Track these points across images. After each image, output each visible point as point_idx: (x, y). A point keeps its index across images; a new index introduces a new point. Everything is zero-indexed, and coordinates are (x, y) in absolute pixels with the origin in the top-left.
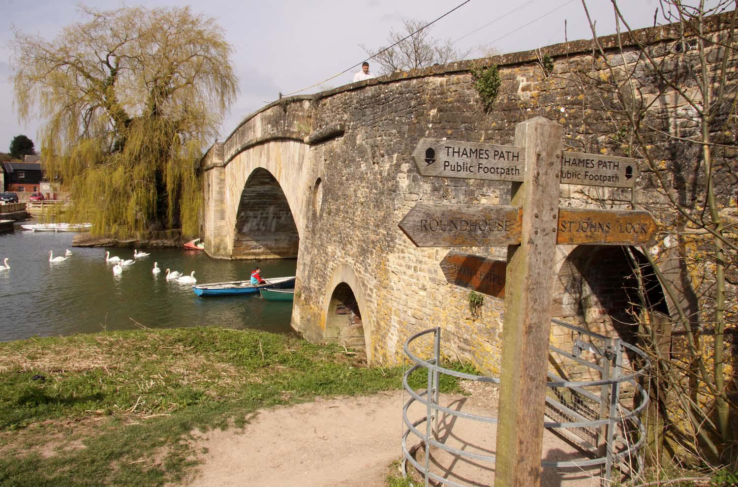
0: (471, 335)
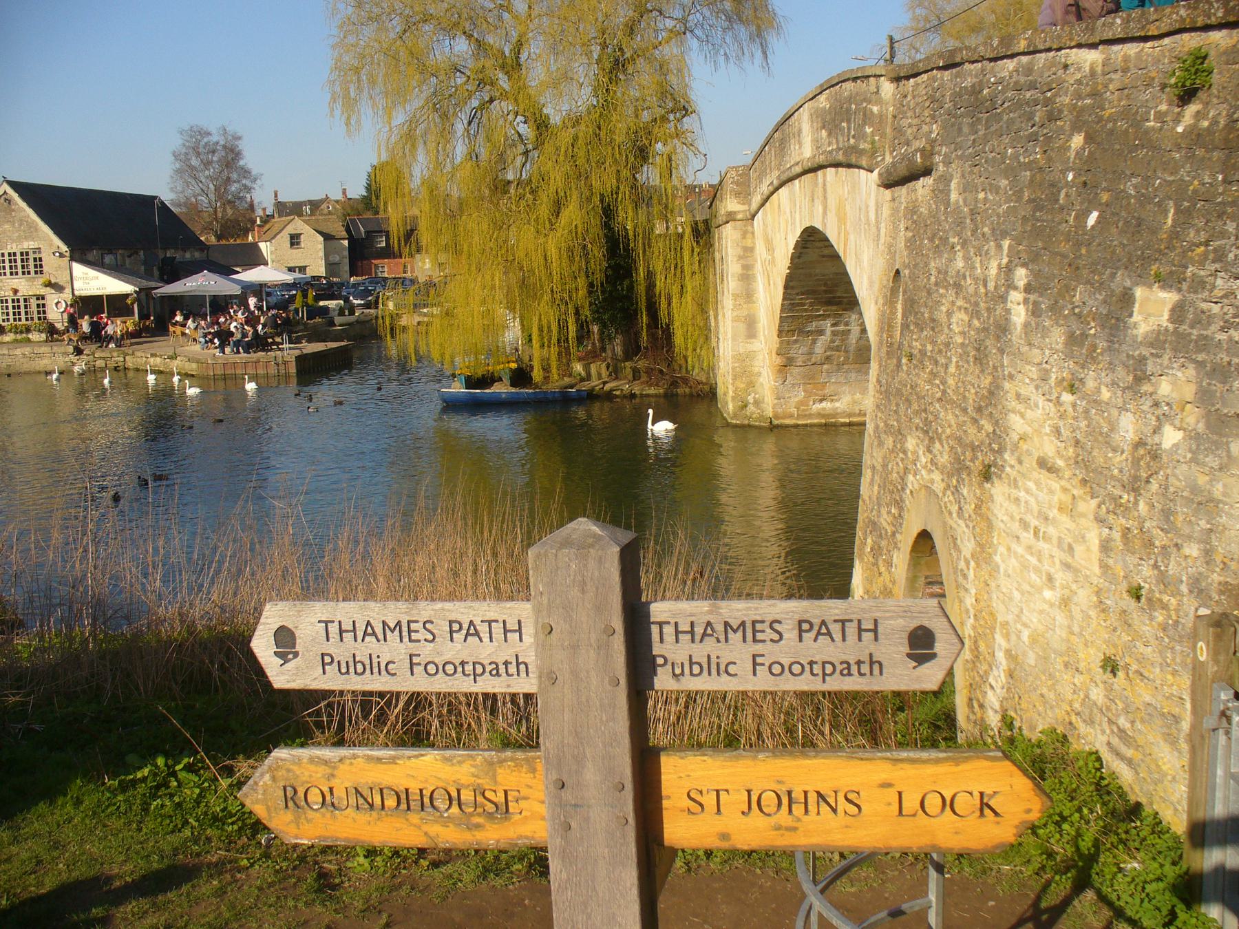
0: (1133, 722)
